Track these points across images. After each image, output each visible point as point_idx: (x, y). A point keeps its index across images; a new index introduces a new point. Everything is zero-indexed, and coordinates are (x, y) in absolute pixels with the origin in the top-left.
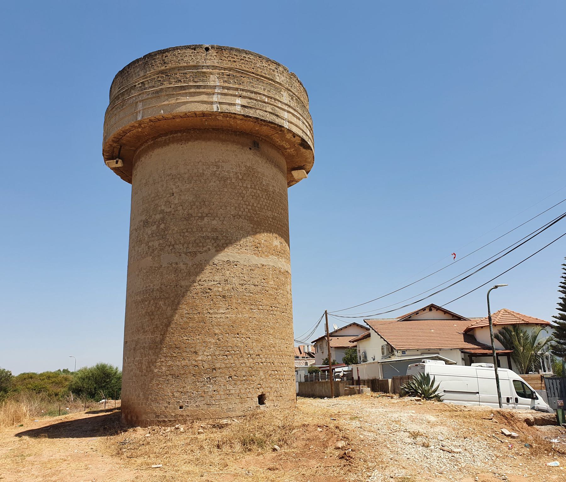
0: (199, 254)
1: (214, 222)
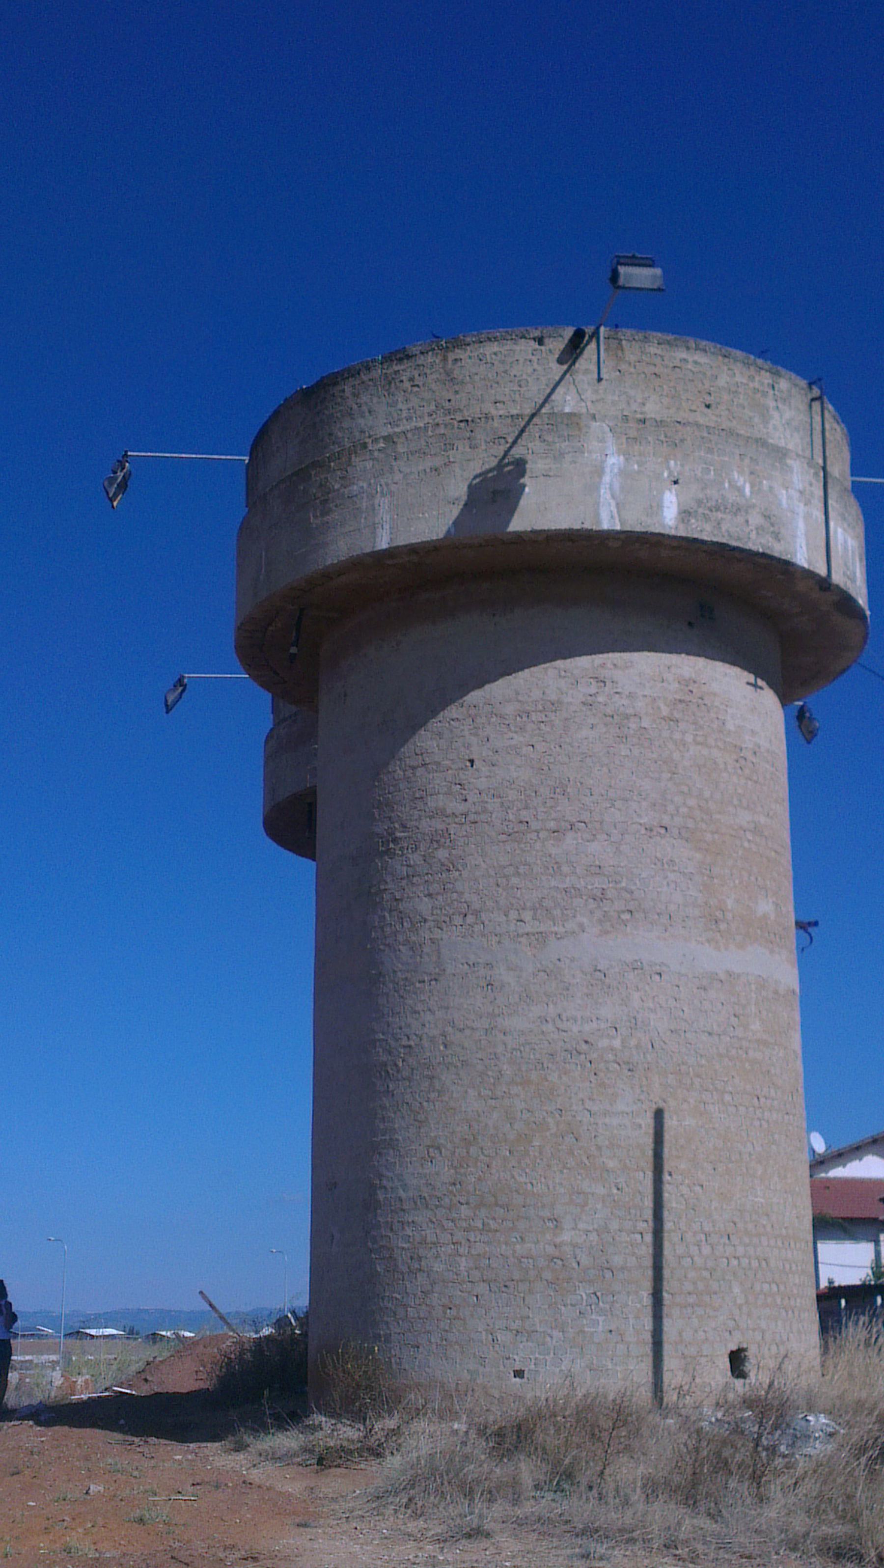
1: (594, 847)
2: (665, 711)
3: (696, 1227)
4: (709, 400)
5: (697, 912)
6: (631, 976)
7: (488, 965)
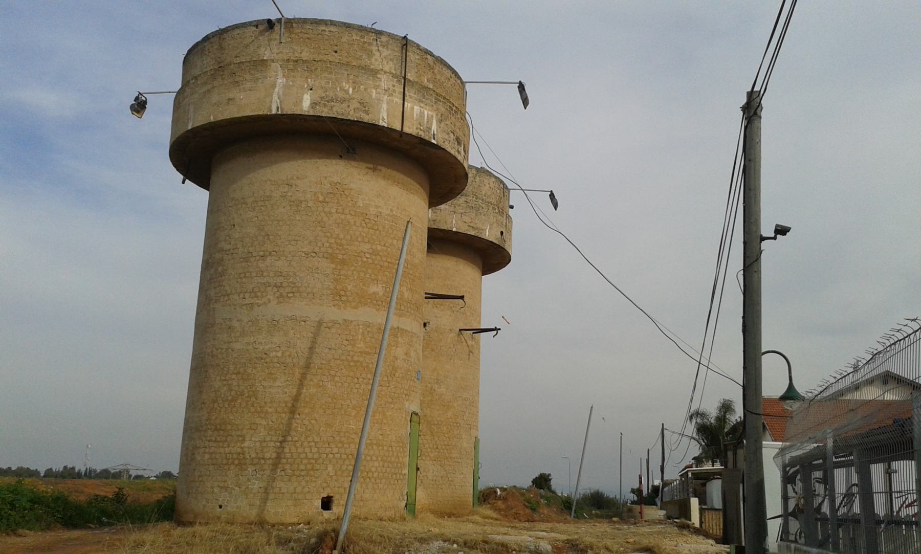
0: (256, 307)
1: (279, 263)
2: (321, 198)
3: (310, 439)
4: (336, 48)
5: (329, 292)
6: (289, 323)
7: (230, 320)
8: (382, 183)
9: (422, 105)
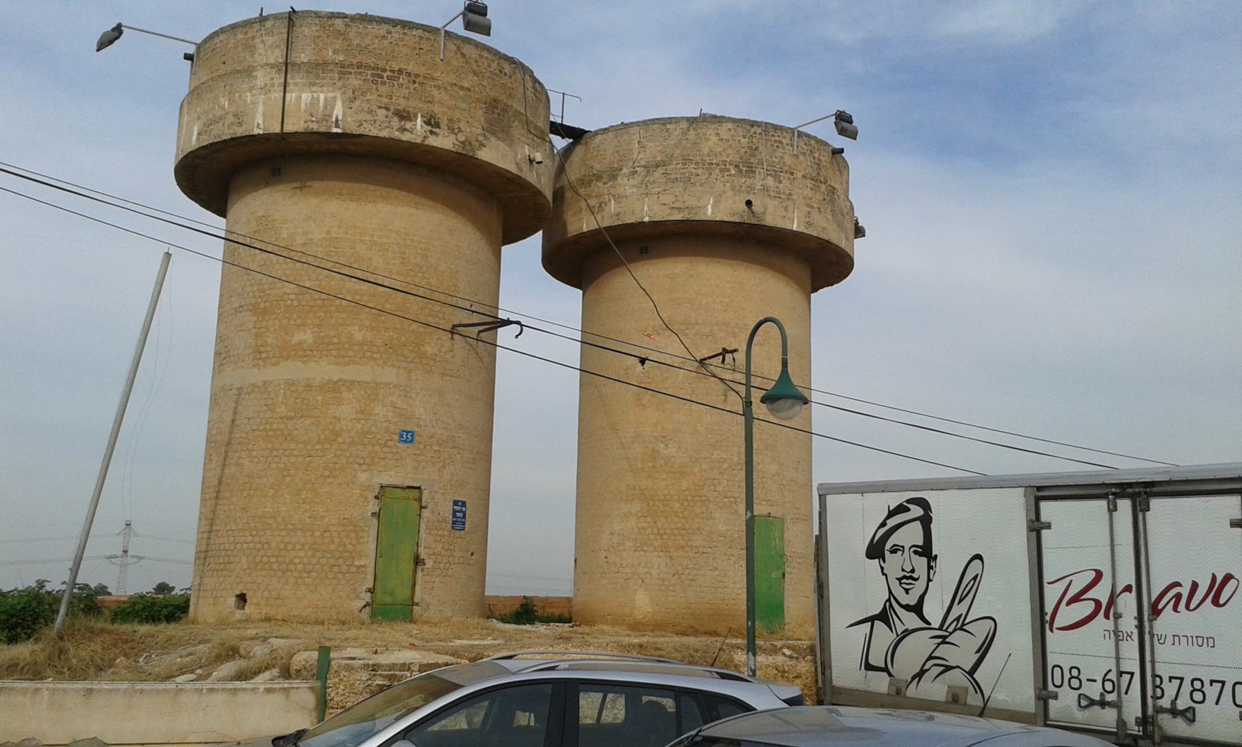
8: (315, 201)
9: (314, 89)
